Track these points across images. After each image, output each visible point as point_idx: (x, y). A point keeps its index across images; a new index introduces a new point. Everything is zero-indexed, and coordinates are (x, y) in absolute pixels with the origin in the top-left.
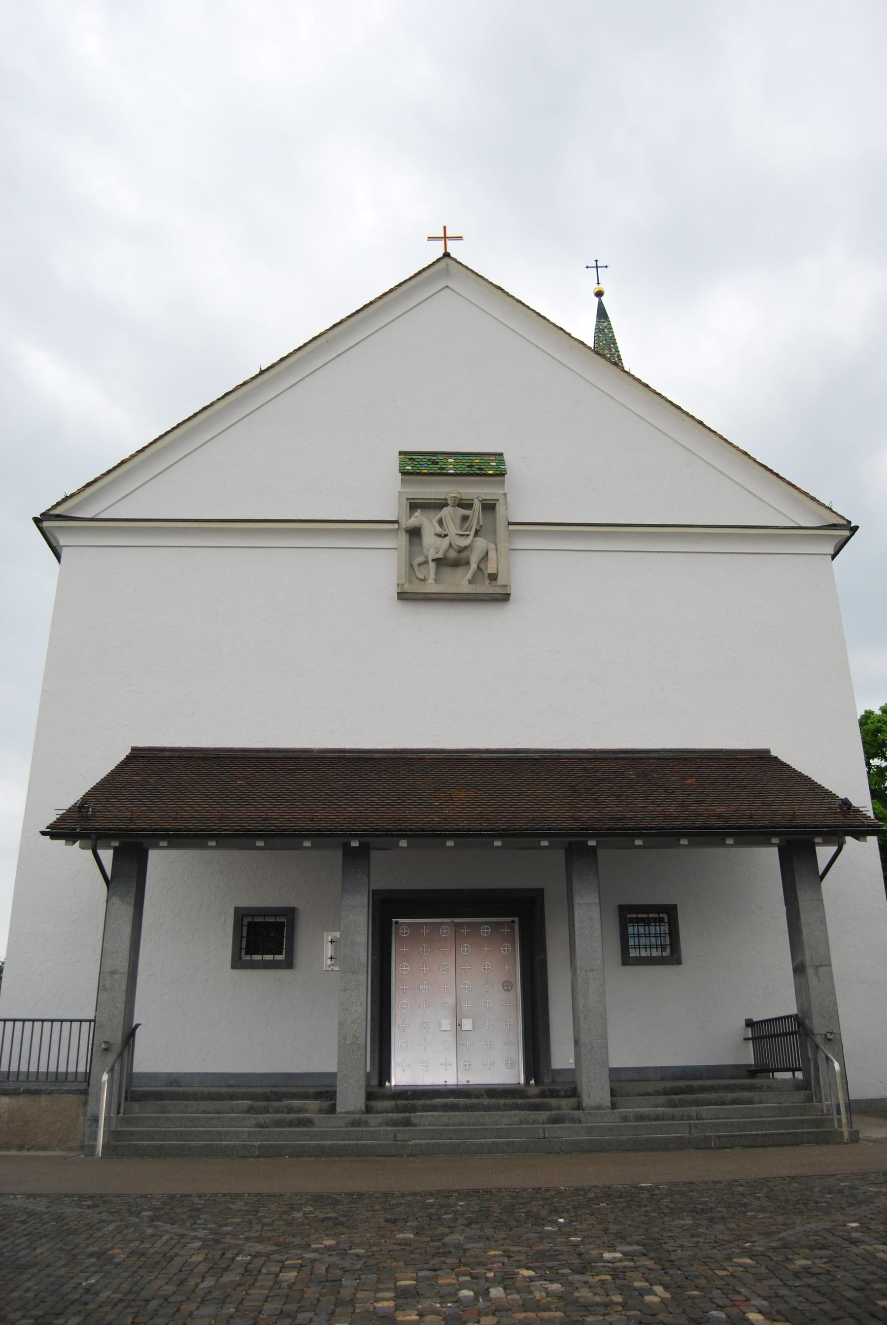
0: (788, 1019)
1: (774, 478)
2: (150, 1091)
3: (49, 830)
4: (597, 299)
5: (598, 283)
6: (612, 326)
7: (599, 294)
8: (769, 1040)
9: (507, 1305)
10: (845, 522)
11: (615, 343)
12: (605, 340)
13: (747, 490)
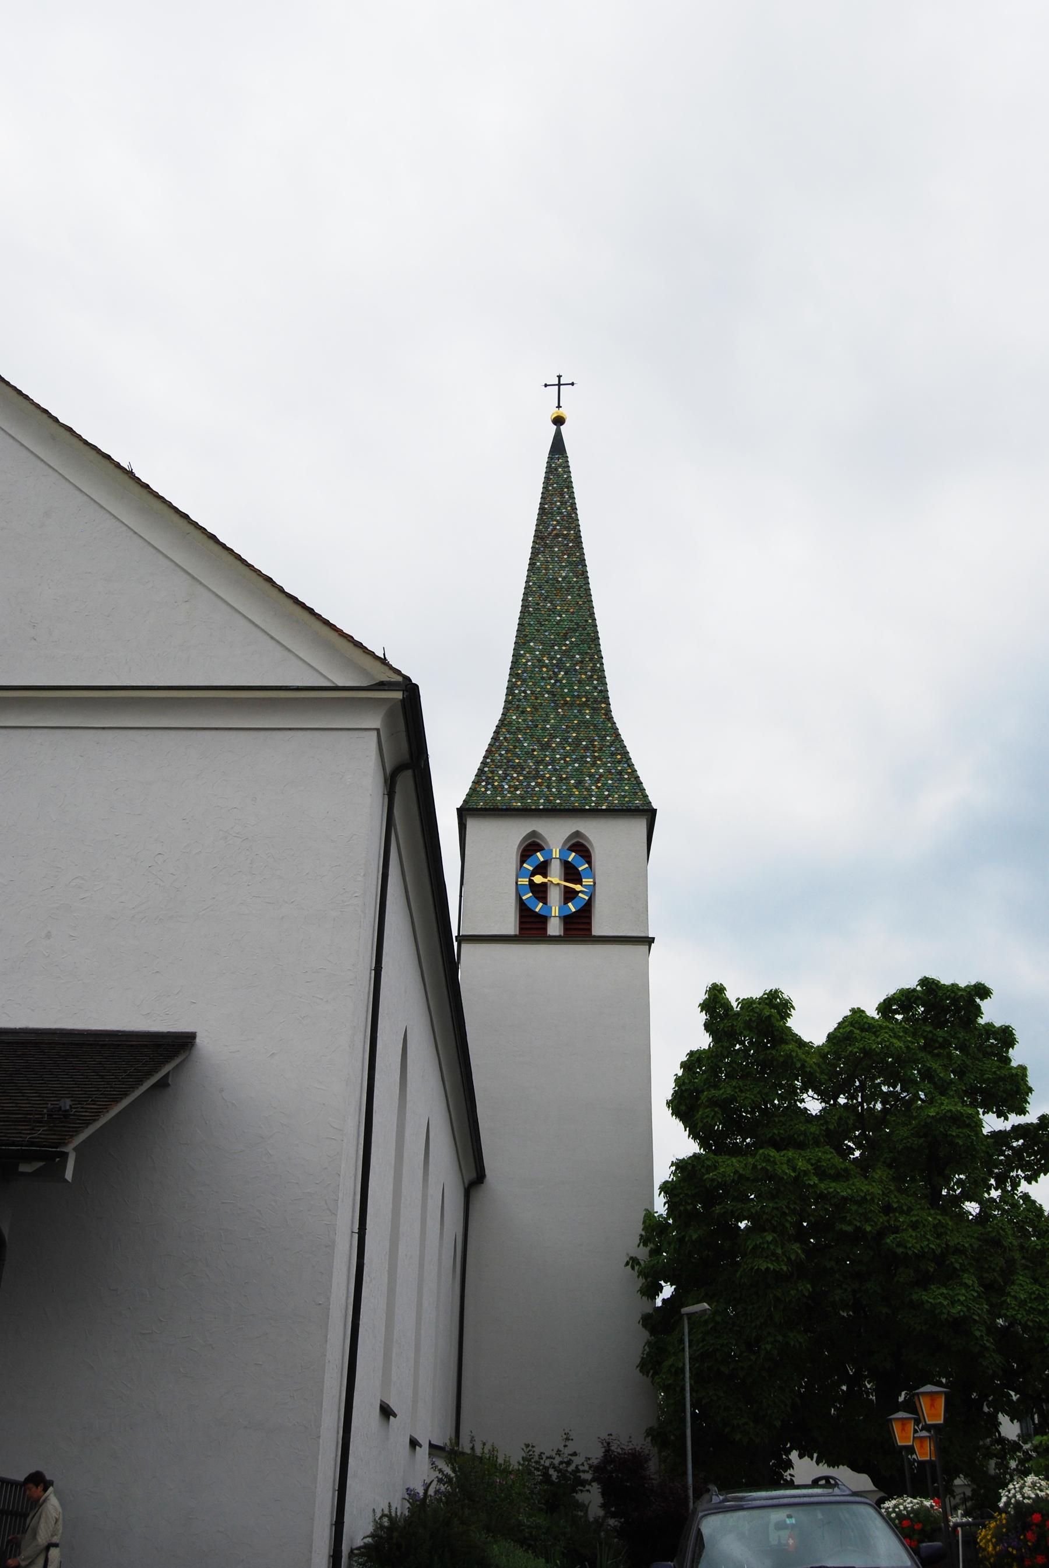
0: (12, 1486)
1: (305, 615)
2: (767, 1490)
5: (559, 407)
6: (570, 464)
7: (559, 421)
8: (16, 1519)
10: (400, 679)
11: (570, 486)
13: (268, 634)
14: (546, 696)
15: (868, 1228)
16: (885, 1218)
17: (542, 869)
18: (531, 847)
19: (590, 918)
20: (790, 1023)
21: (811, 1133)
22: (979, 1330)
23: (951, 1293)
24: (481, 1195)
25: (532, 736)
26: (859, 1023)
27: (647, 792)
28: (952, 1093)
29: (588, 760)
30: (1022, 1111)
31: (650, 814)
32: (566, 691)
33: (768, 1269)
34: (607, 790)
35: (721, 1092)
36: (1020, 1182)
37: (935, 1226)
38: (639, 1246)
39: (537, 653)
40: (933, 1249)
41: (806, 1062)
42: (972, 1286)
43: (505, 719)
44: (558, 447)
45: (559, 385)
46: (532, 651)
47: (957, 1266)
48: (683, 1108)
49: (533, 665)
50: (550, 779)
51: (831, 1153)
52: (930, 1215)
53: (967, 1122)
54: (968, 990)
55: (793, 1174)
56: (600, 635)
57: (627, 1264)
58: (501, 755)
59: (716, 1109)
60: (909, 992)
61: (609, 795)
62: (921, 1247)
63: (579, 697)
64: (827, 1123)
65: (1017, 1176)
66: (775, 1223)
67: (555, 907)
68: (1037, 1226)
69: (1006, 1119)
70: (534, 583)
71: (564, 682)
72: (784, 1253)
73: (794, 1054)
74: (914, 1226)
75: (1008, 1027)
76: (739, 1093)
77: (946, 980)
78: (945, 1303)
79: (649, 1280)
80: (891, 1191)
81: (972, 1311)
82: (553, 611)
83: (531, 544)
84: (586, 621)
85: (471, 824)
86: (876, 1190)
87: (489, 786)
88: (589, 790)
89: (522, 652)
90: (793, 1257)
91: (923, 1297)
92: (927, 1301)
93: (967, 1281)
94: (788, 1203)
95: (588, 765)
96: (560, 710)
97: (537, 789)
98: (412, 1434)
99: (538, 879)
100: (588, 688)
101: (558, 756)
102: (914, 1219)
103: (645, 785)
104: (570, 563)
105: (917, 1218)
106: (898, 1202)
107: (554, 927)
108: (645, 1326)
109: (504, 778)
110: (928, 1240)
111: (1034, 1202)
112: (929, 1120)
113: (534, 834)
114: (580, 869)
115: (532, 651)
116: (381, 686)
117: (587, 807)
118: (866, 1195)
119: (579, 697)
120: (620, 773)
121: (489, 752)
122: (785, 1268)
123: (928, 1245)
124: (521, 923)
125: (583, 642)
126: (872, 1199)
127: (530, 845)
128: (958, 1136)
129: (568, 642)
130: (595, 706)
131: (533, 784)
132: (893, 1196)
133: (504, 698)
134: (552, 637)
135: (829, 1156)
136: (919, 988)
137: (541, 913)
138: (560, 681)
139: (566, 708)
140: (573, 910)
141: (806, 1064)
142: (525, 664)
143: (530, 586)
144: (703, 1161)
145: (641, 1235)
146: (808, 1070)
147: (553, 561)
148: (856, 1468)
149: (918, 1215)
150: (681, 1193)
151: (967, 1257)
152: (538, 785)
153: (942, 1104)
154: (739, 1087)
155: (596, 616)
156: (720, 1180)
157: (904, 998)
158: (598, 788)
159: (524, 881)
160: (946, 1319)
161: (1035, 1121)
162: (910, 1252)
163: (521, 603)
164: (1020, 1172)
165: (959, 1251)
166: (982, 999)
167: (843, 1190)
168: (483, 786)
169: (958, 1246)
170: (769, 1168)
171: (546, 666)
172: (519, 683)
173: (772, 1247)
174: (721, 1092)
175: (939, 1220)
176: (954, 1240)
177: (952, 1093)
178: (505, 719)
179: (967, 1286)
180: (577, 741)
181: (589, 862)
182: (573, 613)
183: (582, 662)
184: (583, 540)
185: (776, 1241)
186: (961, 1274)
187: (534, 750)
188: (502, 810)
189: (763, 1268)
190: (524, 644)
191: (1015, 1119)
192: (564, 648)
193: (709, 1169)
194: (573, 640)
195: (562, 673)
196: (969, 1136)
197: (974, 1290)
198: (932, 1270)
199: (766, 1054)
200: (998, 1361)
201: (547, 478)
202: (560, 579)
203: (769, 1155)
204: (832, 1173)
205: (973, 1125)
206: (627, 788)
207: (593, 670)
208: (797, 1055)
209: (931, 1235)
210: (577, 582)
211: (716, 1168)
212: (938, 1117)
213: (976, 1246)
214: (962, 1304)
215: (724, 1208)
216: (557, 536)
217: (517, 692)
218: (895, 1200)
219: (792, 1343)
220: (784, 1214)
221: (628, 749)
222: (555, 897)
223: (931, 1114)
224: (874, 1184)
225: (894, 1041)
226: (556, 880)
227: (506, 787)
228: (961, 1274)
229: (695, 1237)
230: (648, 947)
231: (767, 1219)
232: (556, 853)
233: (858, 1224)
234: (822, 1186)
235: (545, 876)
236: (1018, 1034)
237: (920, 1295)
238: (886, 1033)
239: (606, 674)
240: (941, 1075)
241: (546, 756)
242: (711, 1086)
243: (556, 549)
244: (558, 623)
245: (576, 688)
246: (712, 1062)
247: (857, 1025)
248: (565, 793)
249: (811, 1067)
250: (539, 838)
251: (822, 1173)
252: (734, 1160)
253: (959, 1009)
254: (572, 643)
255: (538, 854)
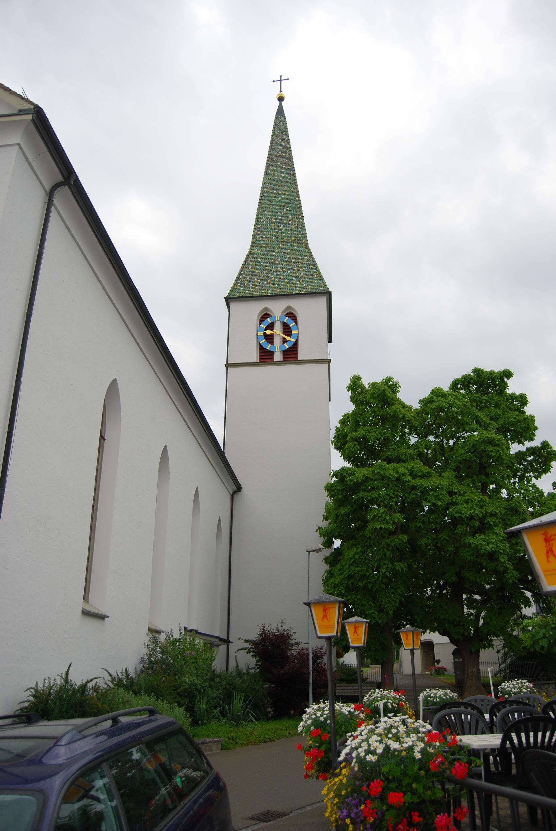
3: (129, 751)
4: (278, 102)
5: (281, 91)
7: (281, 99)
9: (375, 680)
12: (280, 130)
14: (273, 238)
15: (440, 504)
16: (450, 498)
17: (271, 326)
18: (265, 316)
19: (297, 351)
20: (399, 395)
21: (409, 454)
22: (503, 558)
23: (487, 538)
24: (237, 497)
25: (265, 259)
26: (437, 393)
27: (327, 283)
28: (490, 429)
29: (295, 269)
30: (531, 439)
31: (329, 294)
32: (284, 235)
33: (381, 528)
34: (305, 283)
35: (358, 433)
36: (531, 479)
37: (479, 502)
38: (323, 521)
39: (269, 216)
40: (477, 514)
41: (405, 414)
42: (500, 533)
43: (251, 251)
44: (280, 112)
45: (281, 80)
46: (265, 216)
47: (492, 523)
48: (339, 444)
49: (267, 223)
50: (274, 280)
51: (420, 464)
52: (476, 496)
53: (497, 443)
54: (500, 373)
55: (396, 475)
56: (302, 205)
57: (317, 530)
58: (248, 269)
59: (355, 443)
60: (466, 376)
61: (306, 286)
62: (471, 513)
63: (291, 237)
64: (418, 448)
65: (530, 476)
66: (386, 503)
67: (278, 347)
68: (539, 501)
69: (523, 445)
70: (267, 181)
71: (283, 230)
72: (391, 519)
73: (398, 410)
74: (467, 502)
75: (523, 394)
76: (368, 434)
77: (487, 368)
78: (483, 543)
79: (325, 538)
80: (453, 483)
81: (499, 548)
82: (277, 195)
83: (266, 162)
84: (295, 198)
85: (232, 305)
86: (445, 482)
87: (242, 286)
88: (295, 284)
89: (261, 217)
90: (396, 521)
91: (471, 541)
92: (473, 543)
93: (497, 531)
94: (394, 491)
95: (295, 272)
96: (281, 245)
97: (267, 285)
98: (150, 626)
99: (268, 332)
100: (295, 233)
101: (279, 268)
102: (466, 498)
103: (325, 280)
104: (286, 170)
105: (468, 497)
106: (458, 489)
107: (278, 357)
108: (326, 563)
109: (249, 281)
110: (475, 509)
111: (538, 488)
112: (475, 443)
113: (266, 309)
114: (291, 326)
115: (265, 216)
116: (21, 112)
117: (294, 293)
118: (438, 485)
119: (291, 237)
120: (312, 275)
121: (242, 268)
122: (391, 527)
123: (474, 512)
124: (260, 356)
125: (293, 209)
126: (442, 488)
127: (264, 315)
128: (492, 451)
129: (285, 210)
130: (299, 241)
131: (265, 283)
132: (455, 486)
133: (251, 240)
134: (277, 208)
135: (419, 466)
136: (472, 374)
137: (270, 350)
138: (281, 230)
139: (284, 243)
140: (287, 347)
141: (406, 416)
142: (262, 223)
143: (265, 183)
144: (347, 471)
145: (324, 515)
146: (407, 419)
147: (277, 169)
148: (443, 634)
149: (469, 496)
150: (335, 489)
151: (497, 518)
152: (268, 283)
153: (483, 433)
154: (368, 430)
155: (300, 196)
156: (355, 480)
157: (463, 380)
158: (300, 283)
159: (261, 334)
160: (484, 552)
161: (540, 445)
162: (463, 516)
163: (260, 192)
164: (531, 473)
165: (493, 515)
166: (508, 378)
167: (425, 483)
168: (239, 286)
169: (492, 512)
170: (381, 472)
171: (273, 223)
172: (259, 232)
173: (384, 516)
174: (358, 433)
175: (482, 498)
176: (490, 509)
177: (490, 429)
178: (251, 251)
179: (496, 534)
180: (290, 260)
181: (296, 322)
182: (288, 195)
183: (292, 219)
184: (293, 157)
185: (387, 513)
186: (494, 527)
187: (266, 266)
188: (248, 297)
189: (378, 527)
190: (262, 212)
191: (528, 444)
192: (283, 213)
193: (351, 475)
194: (288, 208)
195: (282, 226)
196: (498, 451)
197: (500, 536)
198: (477, 525)
199: (383, 412)
200: (515, 575)
201: (274, 128)
202: (281, 178)
203: (382, 465)
204: (420, 475)
205: (501, 444)
206: (315, 282)
207: (299, 223)
208: (400, 411)
209: (477, 507)
210: (290, 179)
211: (354, 474)
212: (480, 441)
213: (503, 512)
214: (493, 544)
215: (358, 496)
216: (280, 156)
217: (258, 237)
218: (456, 488)
219: (397, 568)
220: (391, 498)
221: (317, 262)
222: (277, 341)
223: (476, 439)
224: (444, 479)
225: (456, 401)
226: (278, 332)
227: (251, 285)
228: (494, 527)
229: (343, 512)
230: (327, 364)
231: (382, 501)
232: (278, 318)
233: (434, 502)
234: (413, 481)
235: (272, 330)
236: (529, 398)
237: (470, 540)
238: (452, 397)
239: (306, 225)
240: (484, 419)
241: (272, 268)
242: (353, 431)
243: (279, 163)
244: (280, 201)
245: (289, 233)
246: (353, 417)
247: (435, 394)
248: (282, 286)
249: (408, 417)
250: (269, 312)
251: (413, 474)
252: (364, 469)
253: (495, 386)
254: (287, 210)
255: (268, 319)
